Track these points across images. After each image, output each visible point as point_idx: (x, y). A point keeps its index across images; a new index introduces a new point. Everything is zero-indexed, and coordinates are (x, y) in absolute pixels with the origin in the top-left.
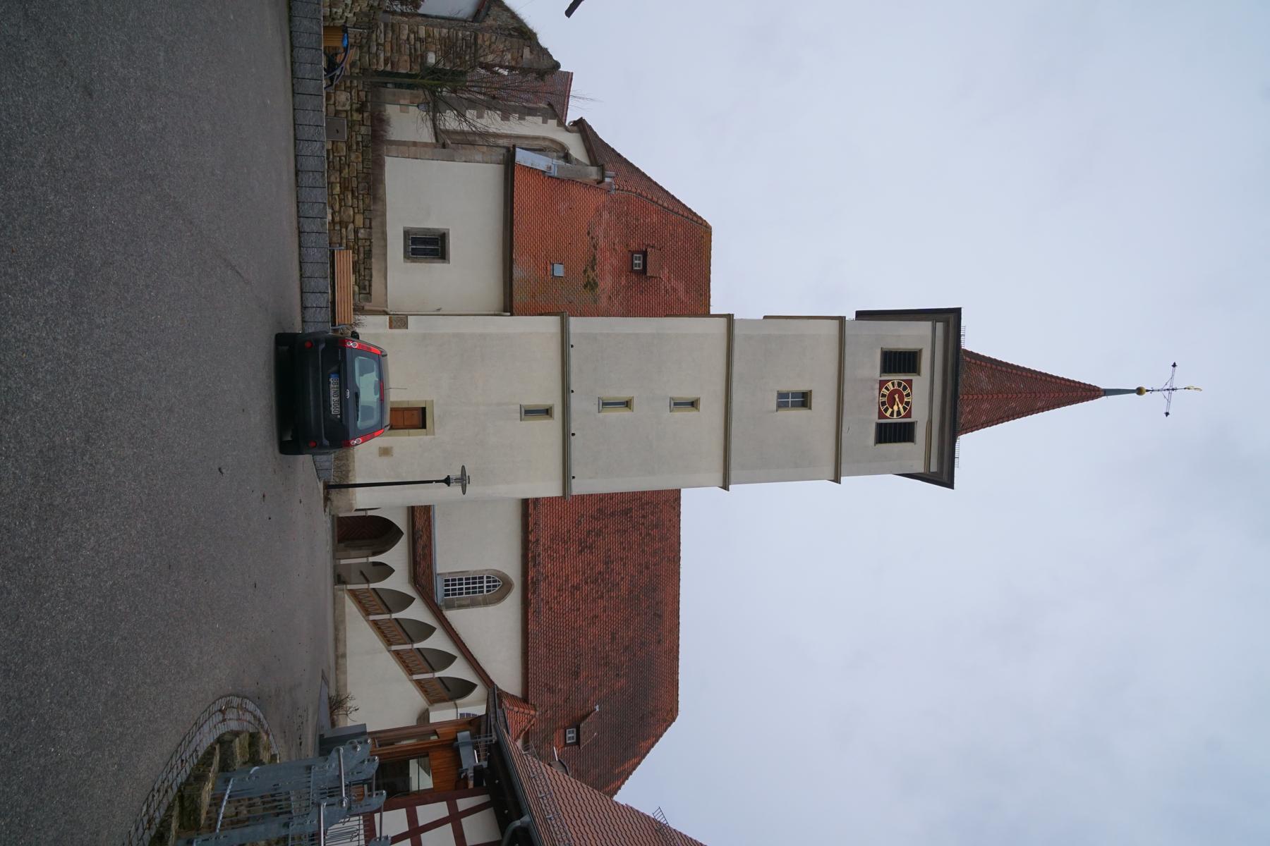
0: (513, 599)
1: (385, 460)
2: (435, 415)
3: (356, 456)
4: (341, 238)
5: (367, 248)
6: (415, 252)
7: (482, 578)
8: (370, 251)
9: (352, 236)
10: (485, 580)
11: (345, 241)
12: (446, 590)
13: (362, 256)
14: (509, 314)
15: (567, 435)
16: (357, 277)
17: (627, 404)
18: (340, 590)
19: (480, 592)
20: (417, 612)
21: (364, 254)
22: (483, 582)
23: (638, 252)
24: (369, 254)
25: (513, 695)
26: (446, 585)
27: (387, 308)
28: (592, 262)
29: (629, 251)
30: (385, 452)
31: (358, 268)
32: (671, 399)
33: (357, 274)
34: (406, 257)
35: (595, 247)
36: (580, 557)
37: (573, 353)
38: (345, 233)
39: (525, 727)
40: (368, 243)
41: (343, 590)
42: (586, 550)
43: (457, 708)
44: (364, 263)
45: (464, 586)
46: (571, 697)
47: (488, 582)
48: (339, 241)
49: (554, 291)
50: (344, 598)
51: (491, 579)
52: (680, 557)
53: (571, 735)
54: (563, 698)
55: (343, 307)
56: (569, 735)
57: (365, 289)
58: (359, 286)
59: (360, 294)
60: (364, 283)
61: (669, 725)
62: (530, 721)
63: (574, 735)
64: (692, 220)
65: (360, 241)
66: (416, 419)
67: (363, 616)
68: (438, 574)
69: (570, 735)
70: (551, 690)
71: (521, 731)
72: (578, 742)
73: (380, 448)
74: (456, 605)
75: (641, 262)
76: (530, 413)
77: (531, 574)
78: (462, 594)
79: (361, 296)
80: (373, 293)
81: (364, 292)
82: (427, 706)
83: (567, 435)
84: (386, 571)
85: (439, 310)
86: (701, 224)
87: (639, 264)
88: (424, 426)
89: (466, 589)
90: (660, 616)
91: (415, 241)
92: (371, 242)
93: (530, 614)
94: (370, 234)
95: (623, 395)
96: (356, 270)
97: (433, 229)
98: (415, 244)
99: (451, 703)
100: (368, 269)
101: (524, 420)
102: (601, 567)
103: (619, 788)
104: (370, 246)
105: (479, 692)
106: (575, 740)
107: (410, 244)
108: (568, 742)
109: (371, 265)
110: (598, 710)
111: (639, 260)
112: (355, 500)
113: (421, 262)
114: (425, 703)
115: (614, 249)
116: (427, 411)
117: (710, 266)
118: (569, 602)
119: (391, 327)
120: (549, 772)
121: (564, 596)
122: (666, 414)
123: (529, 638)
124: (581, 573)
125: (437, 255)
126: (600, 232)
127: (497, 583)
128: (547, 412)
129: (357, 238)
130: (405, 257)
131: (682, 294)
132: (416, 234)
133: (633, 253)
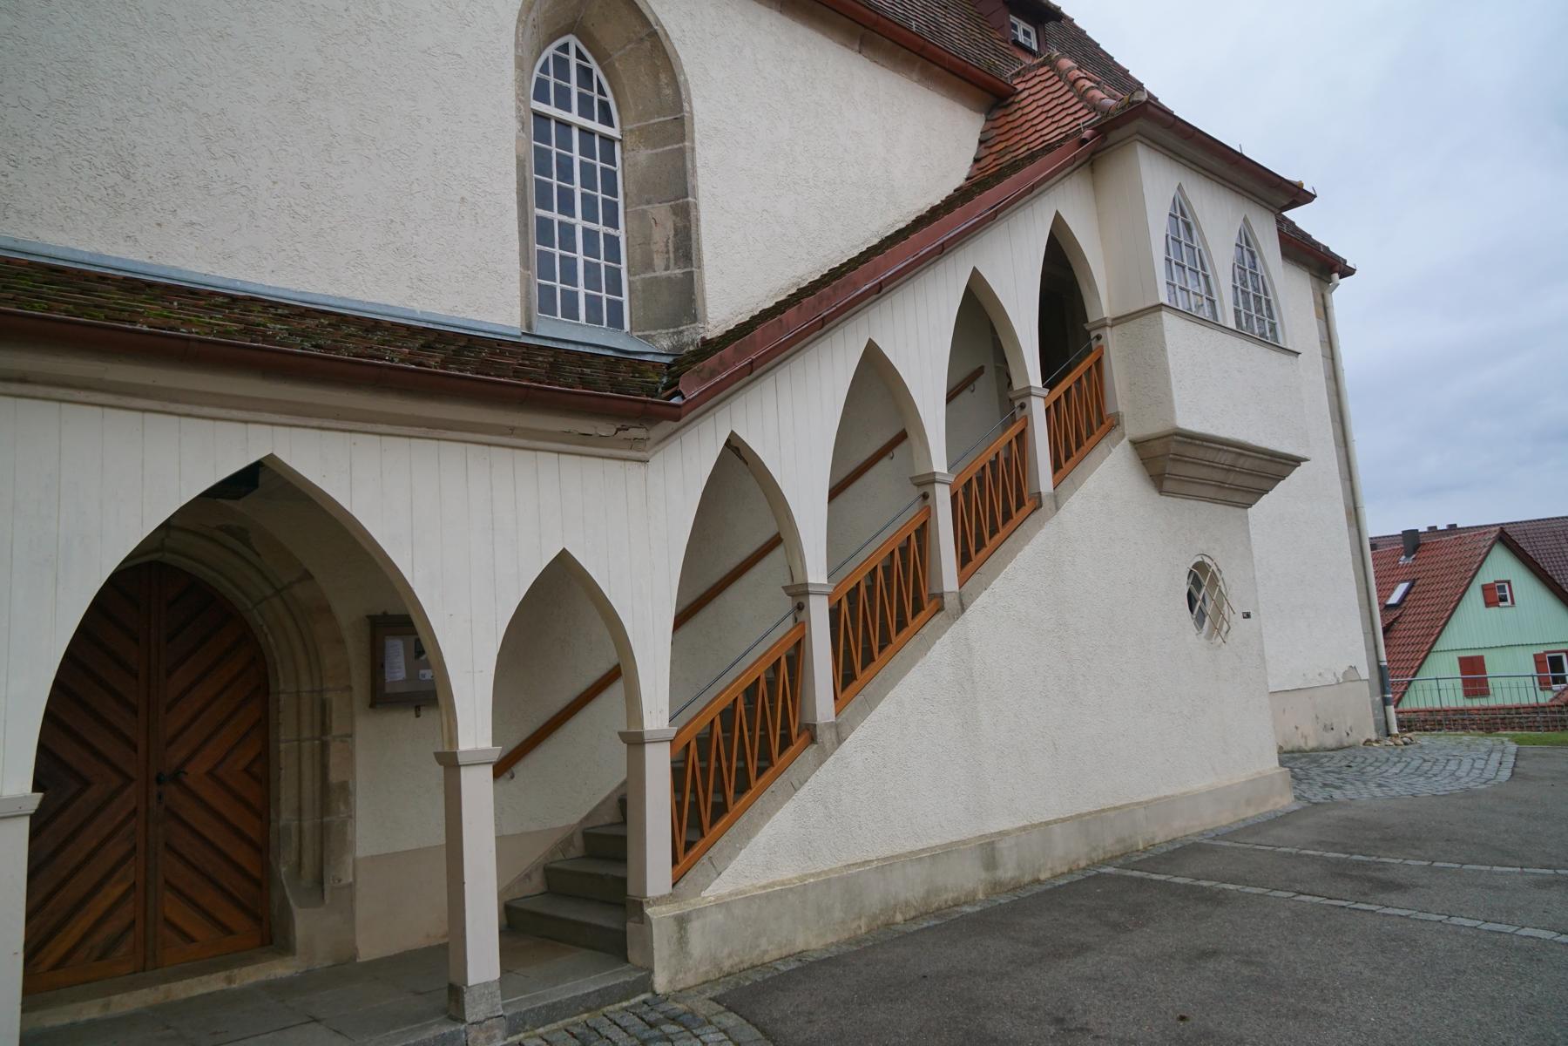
7: (539, 116)
18: (682, 941)
19: (608, 157)
25: (981, 142)
41: (682, 921)
50: (723, 904)
51: (552, 80)
68: (529, 326)
74: (677, 272)
78: (612, 242)
82: (1125, 441)
89: (590, 215)
127: (573, 61)
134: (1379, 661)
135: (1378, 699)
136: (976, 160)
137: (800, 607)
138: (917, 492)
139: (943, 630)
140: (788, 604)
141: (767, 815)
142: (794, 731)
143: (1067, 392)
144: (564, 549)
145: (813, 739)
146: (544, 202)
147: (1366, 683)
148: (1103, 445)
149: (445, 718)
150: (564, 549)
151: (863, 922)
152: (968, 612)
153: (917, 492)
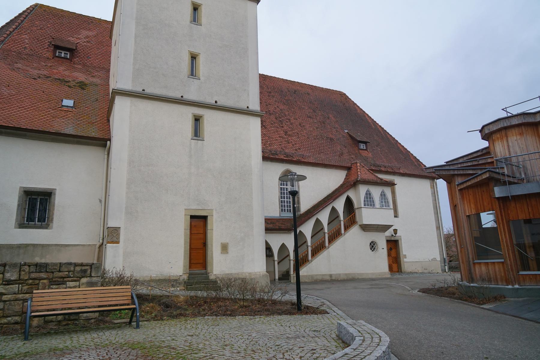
0: (299, 170)
1: (231, 249)
2: (198, 209)
3: (227, 272)
4: (17, 300)
5: (33, 269)
6: (42, 219)
7: (281, 188)
8: (36, 265)
9: (15, 288)
10: (282, 187)
11: (20, 296)
12: (288, 211)
13: (43, 275)
14: (108, 142)
15: (215, 107)
16: (70, 279)
17: (194, 57)
20: (307, 229)
21: (42, 272)
22: (284, 188)
23: (55, 53)
24: (40, 267)
25: (346, 176)
26: (285, 211)
27: (95, 245)
28: (62, 81)
29: (53, 58)
30: (225, 248)
31: (59, 280)
32: (191, 22)
33: (65, 279)
34: (47, 227)
35: (48, 77)
36: (268, 128)
37: (149, 91)
38: (9, 296)
39: (366, 169)
40: (26, 268)
42: (264, 124)
43: (361, 207)
44: (53, 273)
45: (286, 200)
46: (343, 144)
47: (284, 185)
48: (21, 302)
49: (87, 109)
52: (263, 74)
53: (362, 146)
54: (345, 148)
55: (110, 299)
56: (362, 148)
57: (85, 271)
58: (81, 278)
59: (91, 276)
60: (78, 272)
61: (348, 97)
62: (363, 167)
63: (362, 144)
64: (29, 13)
65: (22, 277)
66: (200, 223)
67: (309, 264)
69: (362, 147)
70: (341, 154)
71: (369, 171)
72: (365, 143)
73: (221, 253)
75: (63, 52)
76: (197, 133)
77: (282, 157)
78: (290, 201)
79: (93, 275)
80: (90, 262)
81: (89, 272)
82: (358, 225)
83: (215, 107)
84: (283, 247)
85: (100, 201)
86: (34, 9)
87: (65, 53)
88: (205, 218)
89: (287, 199)
90: (295, 91)
91: (30, 218)
92: (25, 264)
93: (305, 161)
94: (14, 265)
95: (187, 59)
96: (60, 282)
97: (19, 201)
98: (35, 218)
99: (357, 211)
100: (60, 266)
101: (203, 138)
102: (273, 117)
103: (380, 126)
104: (29, 266)
105: (351, 193)
106: (364, 145)
107: (34, 223)
108: (365, 148)
109: (55, 264)
110: (347, 131)
111: (61, 53)
112: (260, 272)
113: (53, 214)
114: (356, 227)
115: (51, 66)
116: (193, 214)
117: (69, 12)
118: (294, 138)
119: (118, 242)
120: (354, 168)
121: (291, 140)
122: (203, 29)
123: (318, 163)
124: (277, 129)
125: (47, 199)
126: (36, 72)
128: (197, 119)
129: (19, 281)
130: (47, 228)
131: (90, 33)
132: (24, 217)
133: (55, 56)
134: (444, 257)
135: (443, 265)
136: (345, 179)
137: (308, 248)
138: (324, 234)
139: (326, 250)
140: (306, 247)
141: (303, 268)
142: (307, 260)
143: (352, 216)
144: (283, 243)
145: (309, 261)
146: (282, 198)
147: (439, 262)
148: (353, 226)
149: (501, 134)
150: (283, 243)
151: (314, 280)
152: (330, 248)
153: (324, 234)
